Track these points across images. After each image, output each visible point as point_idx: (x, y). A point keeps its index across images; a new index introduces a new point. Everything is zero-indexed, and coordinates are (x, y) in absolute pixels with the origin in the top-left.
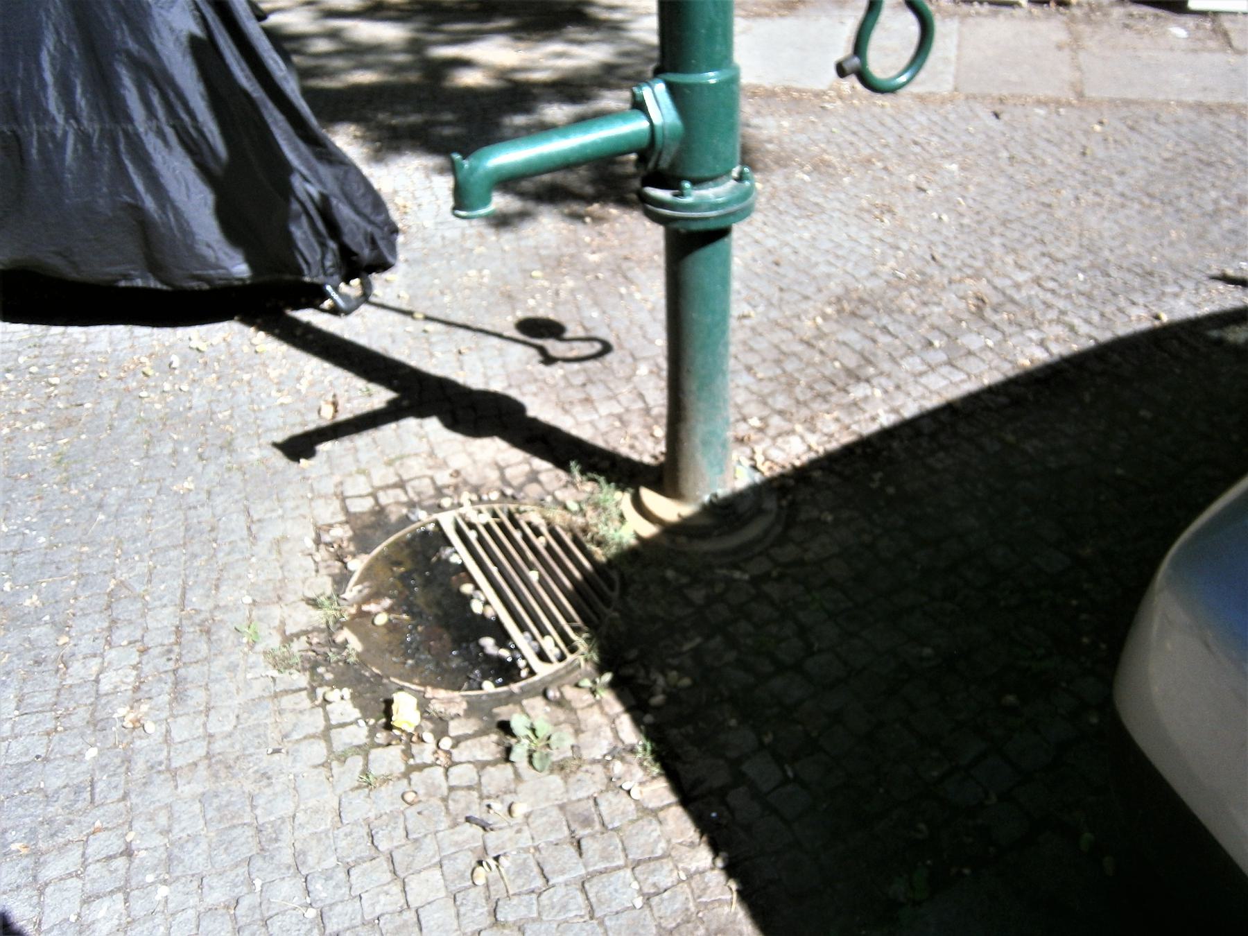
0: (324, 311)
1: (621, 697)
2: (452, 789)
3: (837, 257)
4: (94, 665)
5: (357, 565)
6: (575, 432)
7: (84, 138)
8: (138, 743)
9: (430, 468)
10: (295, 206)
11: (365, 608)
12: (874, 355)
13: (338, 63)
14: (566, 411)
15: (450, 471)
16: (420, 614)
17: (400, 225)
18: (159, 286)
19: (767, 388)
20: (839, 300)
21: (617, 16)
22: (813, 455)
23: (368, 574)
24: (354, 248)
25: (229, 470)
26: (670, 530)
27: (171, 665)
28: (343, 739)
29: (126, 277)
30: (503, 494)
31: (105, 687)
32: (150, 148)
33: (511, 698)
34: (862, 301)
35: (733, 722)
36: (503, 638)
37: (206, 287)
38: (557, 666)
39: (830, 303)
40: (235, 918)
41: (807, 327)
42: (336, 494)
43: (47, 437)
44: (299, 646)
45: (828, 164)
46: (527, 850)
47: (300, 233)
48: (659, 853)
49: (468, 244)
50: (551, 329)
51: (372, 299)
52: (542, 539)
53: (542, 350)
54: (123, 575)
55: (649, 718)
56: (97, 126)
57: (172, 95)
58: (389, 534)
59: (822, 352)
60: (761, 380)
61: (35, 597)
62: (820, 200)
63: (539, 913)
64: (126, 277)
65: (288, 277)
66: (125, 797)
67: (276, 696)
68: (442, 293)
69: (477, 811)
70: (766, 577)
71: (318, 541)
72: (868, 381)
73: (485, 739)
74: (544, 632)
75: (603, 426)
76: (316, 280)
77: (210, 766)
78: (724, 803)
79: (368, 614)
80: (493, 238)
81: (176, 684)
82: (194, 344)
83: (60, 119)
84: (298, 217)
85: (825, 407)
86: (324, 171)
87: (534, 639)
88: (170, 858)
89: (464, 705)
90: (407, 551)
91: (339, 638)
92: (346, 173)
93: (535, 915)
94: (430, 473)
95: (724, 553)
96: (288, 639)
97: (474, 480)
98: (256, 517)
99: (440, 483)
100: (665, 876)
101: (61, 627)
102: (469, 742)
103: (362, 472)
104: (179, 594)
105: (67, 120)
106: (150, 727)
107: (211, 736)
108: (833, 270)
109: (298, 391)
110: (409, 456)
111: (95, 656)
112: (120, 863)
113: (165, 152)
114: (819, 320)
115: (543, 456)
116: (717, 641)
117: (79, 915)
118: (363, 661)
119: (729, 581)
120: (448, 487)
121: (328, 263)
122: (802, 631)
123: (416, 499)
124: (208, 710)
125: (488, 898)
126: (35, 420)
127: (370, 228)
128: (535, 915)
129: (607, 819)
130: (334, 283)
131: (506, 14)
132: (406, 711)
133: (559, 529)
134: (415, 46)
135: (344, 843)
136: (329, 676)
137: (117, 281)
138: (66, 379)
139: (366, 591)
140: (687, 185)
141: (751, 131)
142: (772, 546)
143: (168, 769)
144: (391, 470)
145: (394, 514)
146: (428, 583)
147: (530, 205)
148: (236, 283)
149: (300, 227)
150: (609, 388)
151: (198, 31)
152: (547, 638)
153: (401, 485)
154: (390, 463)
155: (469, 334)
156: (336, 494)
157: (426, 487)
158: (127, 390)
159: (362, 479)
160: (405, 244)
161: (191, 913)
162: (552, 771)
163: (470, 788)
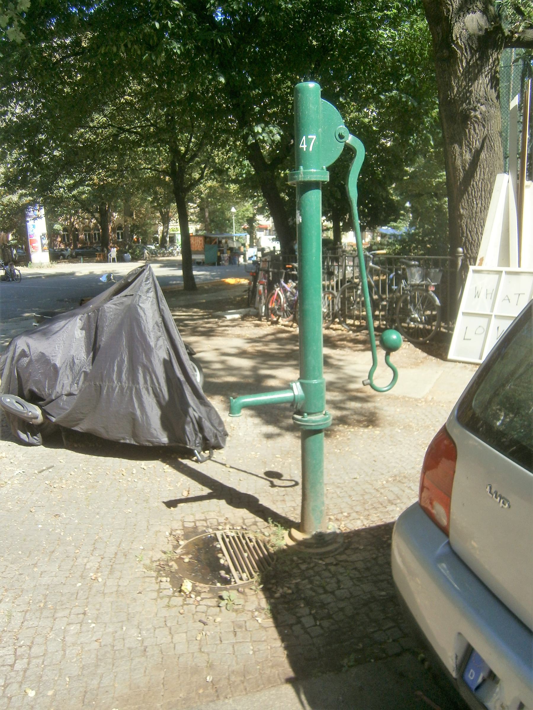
0: (193, 461)
1: (264, 594)
2: (197, 612)
3: (401, 461)
4: (86, 560)
5: (182, 543)
6: (275, 510)
7: (122, 388)
8: (95, 584)
9: (218, 516)
10: (189, 419)
11: (182, 557)
12: (402, 496)
13: (222, 373)
14: (274, 503)
15: (224, 518)
16: (201, 561)
17: (229, 434)
18: (135, 443)
19: (354, 503)
20: (395, 476)
21: (341, 363)
22: (364, 527)
23: (186, 547)
24: (208, 438)
25: (145, 508)
26: (300, 543)
27: (111, 564)
28: (165, 592)
29: (124, 439)
30: (242, 528)
31: (88, 566)
32: (143, 393)
33: (226, 589)
34: (405, 477)
35: (302, 605)
36: (228, 571)
37: (151, 445)
38: (245, 582)
39: (391, 477)
40: (114, 637)
41: (378, 484)
42: (181, 520)
43: (85, 490)
44: (155, 564)
45: (410, 426)
46: (217, 632)
47: (189, 429)
48: (263, 639)
49: (255, 443)
50: (278, 476)
51: (212, 459)
52: (252, 543)
53: (271, 482)
54: (101, 535)
55: (272, 601)
56: (127, 385)
57: (154, 377)
58: (197, 535)
59: (381, 493)
60: (354, 500)
61: (71, 538)
62: (401, 439)
63: (216, 651)
64: (124, 439)
65: (181, 445)
66: (87, 598)
67: (144, 577)
68: (239, 459)
69: (204, 619)
70: (331, 564)
71: (171, 534)
72: (395, 505)
73: (213, 600)
74: (243, 571)
75: (287, 510)
76: (191, 448)
77: (117, 594)
78: (291, 629)
79: (183, 559)
80: (265, 442)
81: (111, 569)
82: (142, 466)
83: (116, 382)
84: (189, 423)
85: (376, 512)
86: (202, 408)
87: (240, 573)
88: (98, 617)
89: (208, 589)
90: (202, 542)
91: (170, 564)
92: (210, 410)
93: (214, 651)
94: (217, 518)
95: (317, 554)
96: (152, 562)
97: (232, 522)
98: (151, 523)
99: (220, 521)
100: (263, 647)
101: (77, 547)
102: (207, 600)
103: (192, 514)
104: (119, 543)
105: (118, 382)
106: (100, 580)
107: (119, 586)
108: (397, 465)
109: (176, 486)
110: (211, 511)
111: (86, 557)
112: (81, 616)
113: (147, 395)
114: (385, 482)
115: (260, 517)
116: (306, 581)
117: (65, 628)
118: (177, 572)
119: (316, 564)
120: (222, 523)
121: (197, 442)
122: (338, 582)
123: (210, 525)
124: (120, 578)
125: (200, 644)
126: (81, 485)
127: (215, 431)
128: (214, 651)
129: (248, 627)
130: (199, 450)
131: (295, 359)
132: (187, 585)
133: (259, 541)
134: (254, 369)
135: (156, 622)
136: (164, 575)
137: (120, 440)
138: (95, 473)
139: (184, 552)
140: (306, 414)
141: (383, 412)
142: (337, 554)
143: (103, 593)
144: (203, 515)
145: (200, 529)
146: (206, 552)
147: (283, 432)
148: (162, 445)
149: (189, 427)
150: (293, 497)
151: (167, 358)
152: (245, 574)
153: (206, 520)
154: (203, 513)
155: (246, 474)
156: (181, 520)
157: (215, 522)
158: (115, 479)
159: (192, 516)
160: (230, 441)
161: (101, 633)
162: (233, 611)
163: (203, 612)
